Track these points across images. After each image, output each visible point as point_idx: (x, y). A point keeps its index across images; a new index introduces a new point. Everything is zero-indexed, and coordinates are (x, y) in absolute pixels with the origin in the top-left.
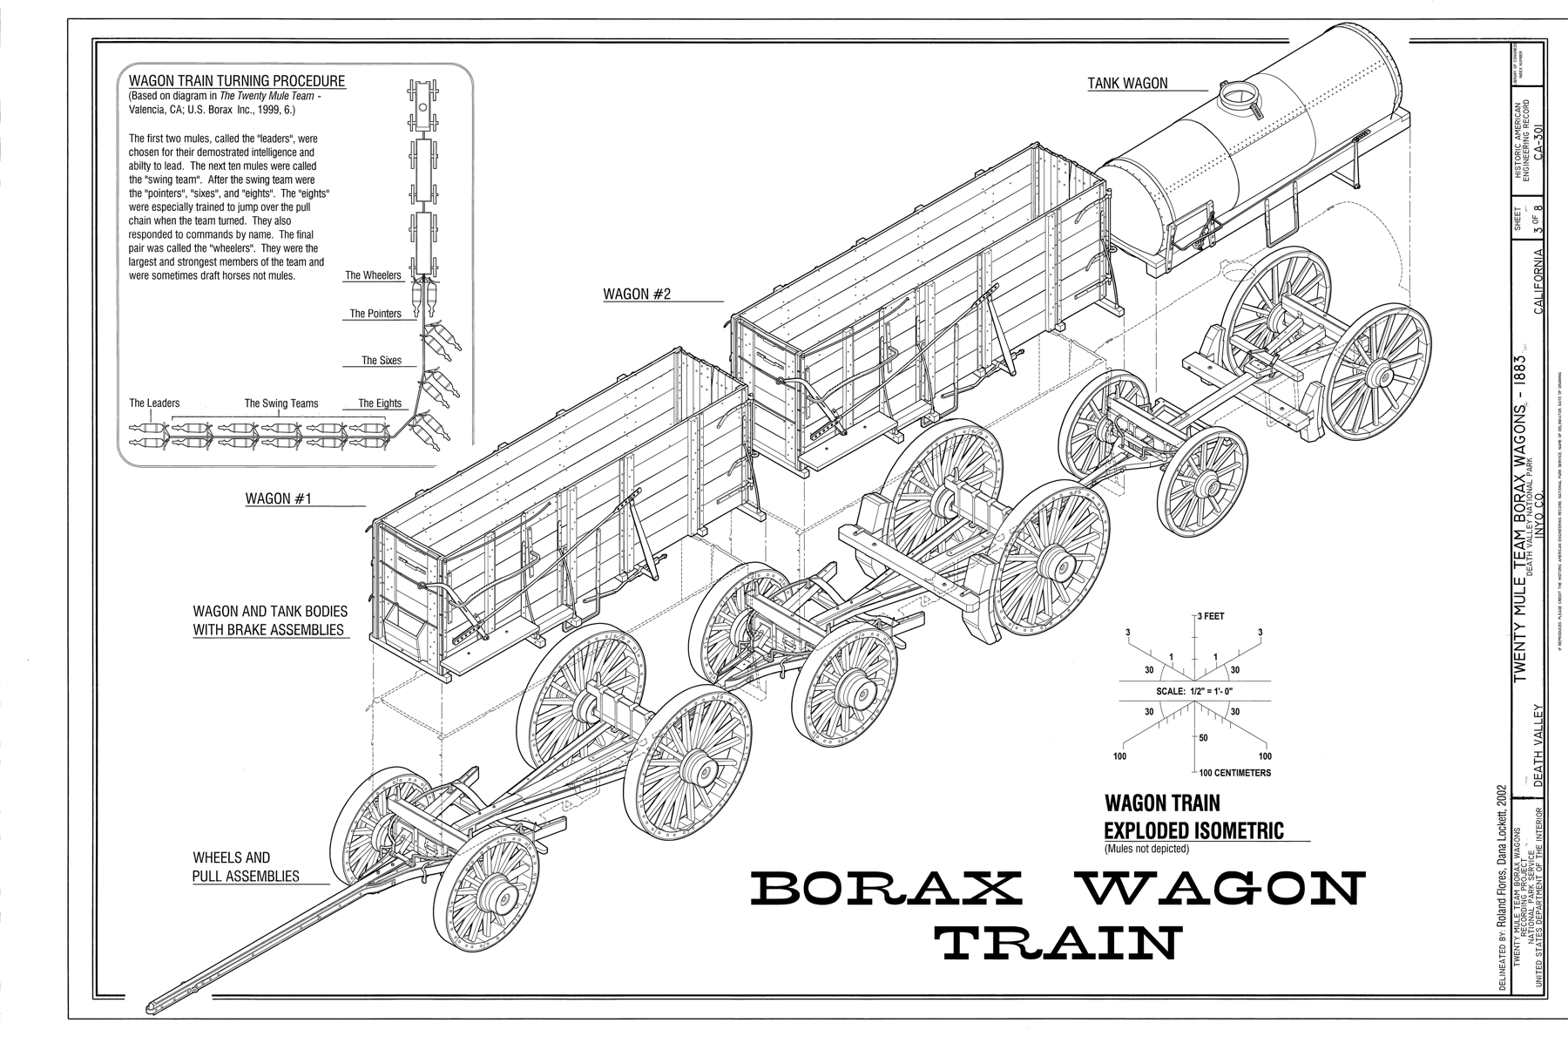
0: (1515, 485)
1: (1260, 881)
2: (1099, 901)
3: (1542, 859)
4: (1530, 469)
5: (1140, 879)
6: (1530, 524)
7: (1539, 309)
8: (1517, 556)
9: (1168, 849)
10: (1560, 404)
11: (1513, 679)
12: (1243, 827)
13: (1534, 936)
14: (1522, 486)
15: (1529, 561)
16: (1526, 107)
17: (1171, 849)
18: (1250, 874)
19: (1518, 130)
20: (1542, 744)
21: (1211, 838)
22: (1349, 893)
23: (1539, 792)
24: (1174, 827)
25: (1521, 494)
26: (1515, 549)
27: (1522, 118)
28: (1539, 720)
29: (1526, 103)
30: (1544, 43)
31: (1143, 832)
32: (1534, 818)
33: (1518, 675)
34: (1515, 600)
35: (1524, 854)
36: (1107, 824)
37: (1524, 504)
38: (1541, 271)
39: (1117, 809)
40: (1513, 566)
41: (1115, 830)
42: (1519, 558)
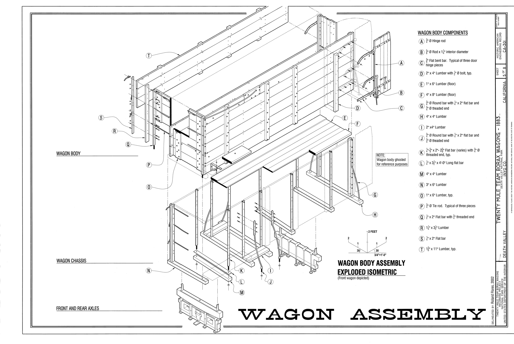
0: (497, 159)
1: (300, 312)
2: (247, 318)
3: (506, 281)
4: (502, 153)
5: (260, 311)
6: (502, 171)
7: (505, 101)
8: (497, 182)
9: (362, 278)
10: (512, 132)
11: (496, 222)
12: (383, 271)
13: (503, 307)
14: (499, 159)
15: (501, 184)
16: (500, 35)
17: (363, 278)
18: (296, 310)
19: (498, 42)
20: (506, 244)
21: (373, 275)
22: (329, 316)
23: (505, 259)
24: (360, 271)
25: (499, 162)
26: (497, 180)
27: (499, 38)
28: (505, 236)
29: (500, 34)
30: (506, 14)
31: (350, 273)
32: (503, 268)
33: (498, 221)
34: (497, 196)
35: (500, 280)
36: (338, 270)
37: (500, 165)
38: (505, 89)
39: (342, 265)
40: (496, 185)
41: (341, 272)
42: (498, 183)
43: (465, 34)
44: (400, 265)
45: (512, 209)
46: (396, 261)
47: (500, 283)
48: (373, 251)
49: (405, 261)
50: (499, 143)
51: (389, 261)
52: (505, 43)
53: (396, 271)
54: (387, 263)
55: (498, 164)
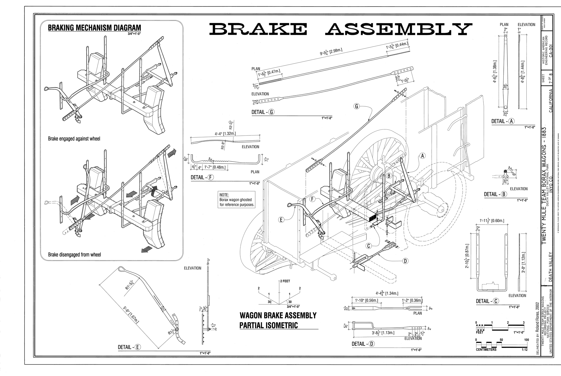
0: (542, 173)
4: (548, 168)
6: (548, 188)
7: (551, 111)
8: (543, 199)
12: (283, 324)
13: (549, 335)
14: (545, 174)
15: (547, 201)
16: (546, 38)
21: (272, 328)
23: (551, 284)
25: (544, 177)
26: (542, 196)
27: (545, 42)
29: (546, 37)
30: (553, 15)
33: (543, 242)
34: (542, 215)
35: (545, 306)
37: (546, 180)
38: (552, 97)
39: (244, 318)
40: (541, 202)
45: (558, 228)
47: (545, 310)
50: (544, 156)
55: (544, 179)
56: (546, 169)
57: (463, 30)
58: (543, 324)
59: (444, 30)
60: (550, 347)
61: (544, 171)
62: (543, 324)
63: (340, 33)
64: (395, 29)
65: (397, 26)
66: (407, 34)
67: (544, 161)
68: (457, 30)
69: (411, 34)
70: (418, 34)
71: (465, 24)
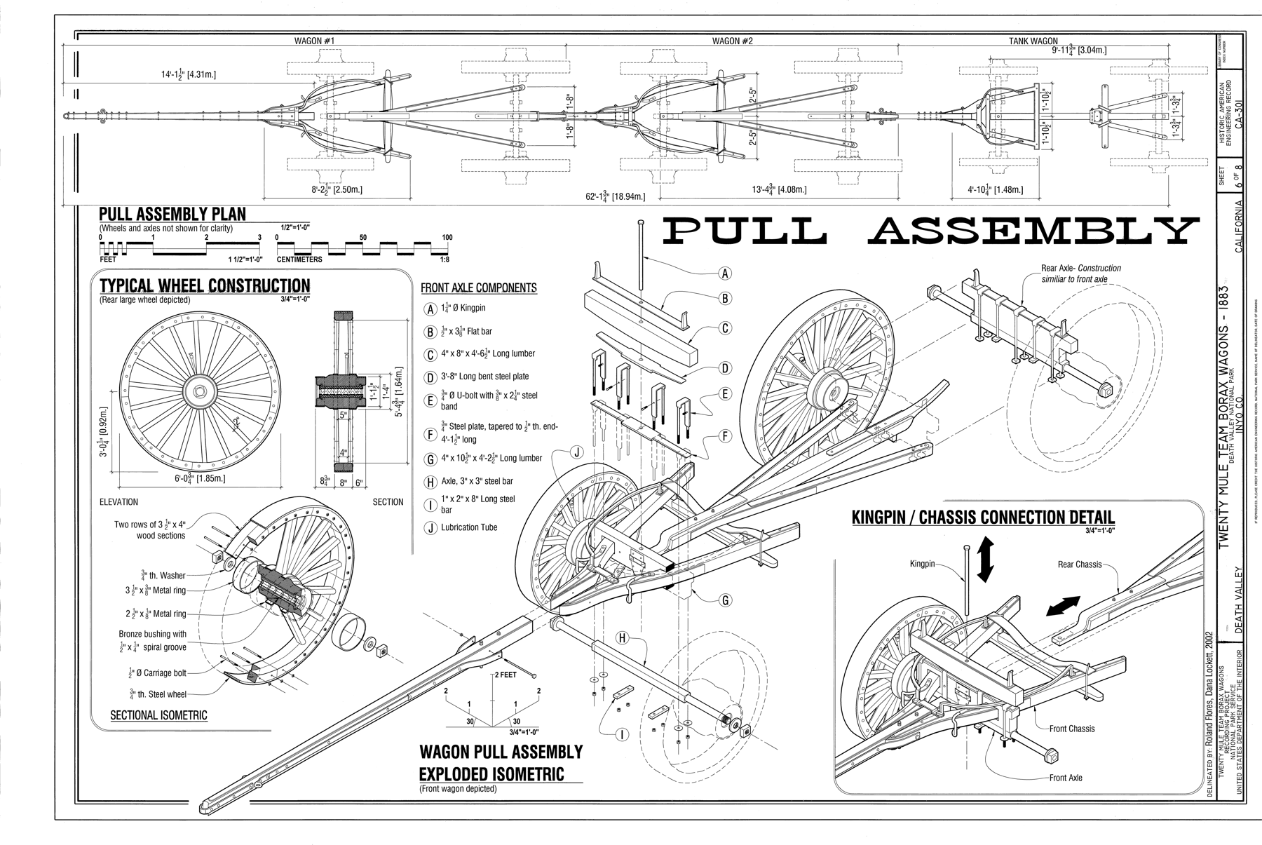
0: (1219, 390)
4: (1232, 377)
6: (1232, 421)
7: (1239, 249)
8: (1221, 447)
12: (532, 771)
13: (1236, 754)
14: (1226, 391)
15: (1231, 451)
16: (1229, 87)
17: (482, 789)
19: (1222, 104)
20: (1242, 599)
21: (506, 780)
23: (1239, 637)
25: (1225, 397)
26: (1219, 442)
27: (1225, 94)
28: (1239, 579)
29: (1229, 83)
30: (1243, 34)
31: (450, 776)
32: (1236, 658)
33: (1222, 543)
34: (1219, 482)
35: (1227, 687)
36: (421, 769)
37: (1227, 405)
38: (1241, 218)
39: (429, 757)
40: (1218, 455)
41: (428, 774)
42: (1223, 449)
43: (530, 290)
44: (569, 757)
45: (1256, 514)
46: (560, 746)
47: (1227, 696)
48: (507, 723)
49: (581, 746)
50: (1224, 352)
51: (544, 746)
52: (1240, 105)
53: (563, 770)
54: (538, 751)
55: (1223, 403)
56: (1228, 380)
57: (1177, 233)
58: (1221, 729)
59: (1136, 232)
60: (1239, 781)
61: (1223, 385)
62: (1221, 729)
63: (901, 241)
64: (1026, 231)
65: (1030, 224)
66: (1052, 241)
67: (1224, 362)
68: (1165, 233)
69: (1062, 241)
70: (1077, 242)
71: (1183, 219)
